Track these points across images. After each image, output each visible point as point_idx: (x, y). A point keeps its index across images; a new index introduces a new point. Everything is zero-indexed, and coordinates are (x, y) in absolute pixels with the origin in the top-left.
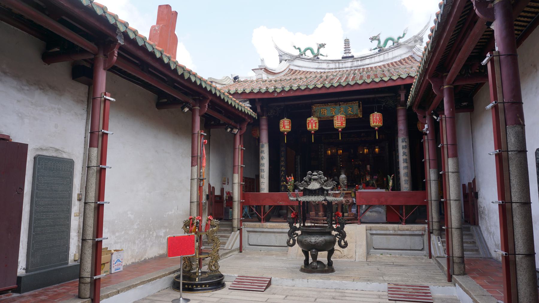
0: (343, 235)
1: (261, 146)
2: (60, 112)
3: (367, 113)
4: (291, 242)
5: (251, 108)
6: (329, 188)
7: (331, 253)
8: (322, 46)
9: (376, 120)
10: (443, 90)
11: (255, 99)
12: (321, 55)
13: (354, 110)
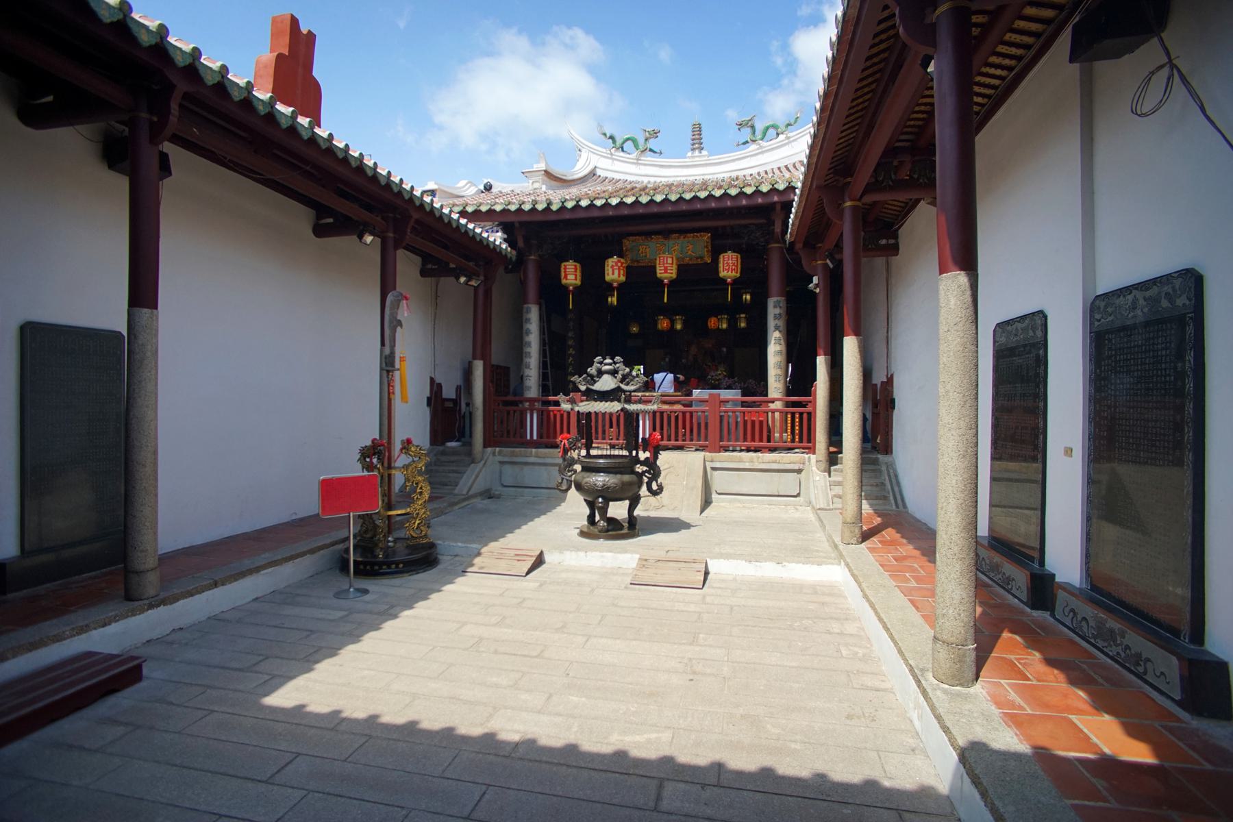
0: (655, 472)
3: (716, 252)
5: (505, 240)
6: (632, 388)
8: (655, 134)
9: (729, 267)
10: (843, 210)
13: (696, 247)
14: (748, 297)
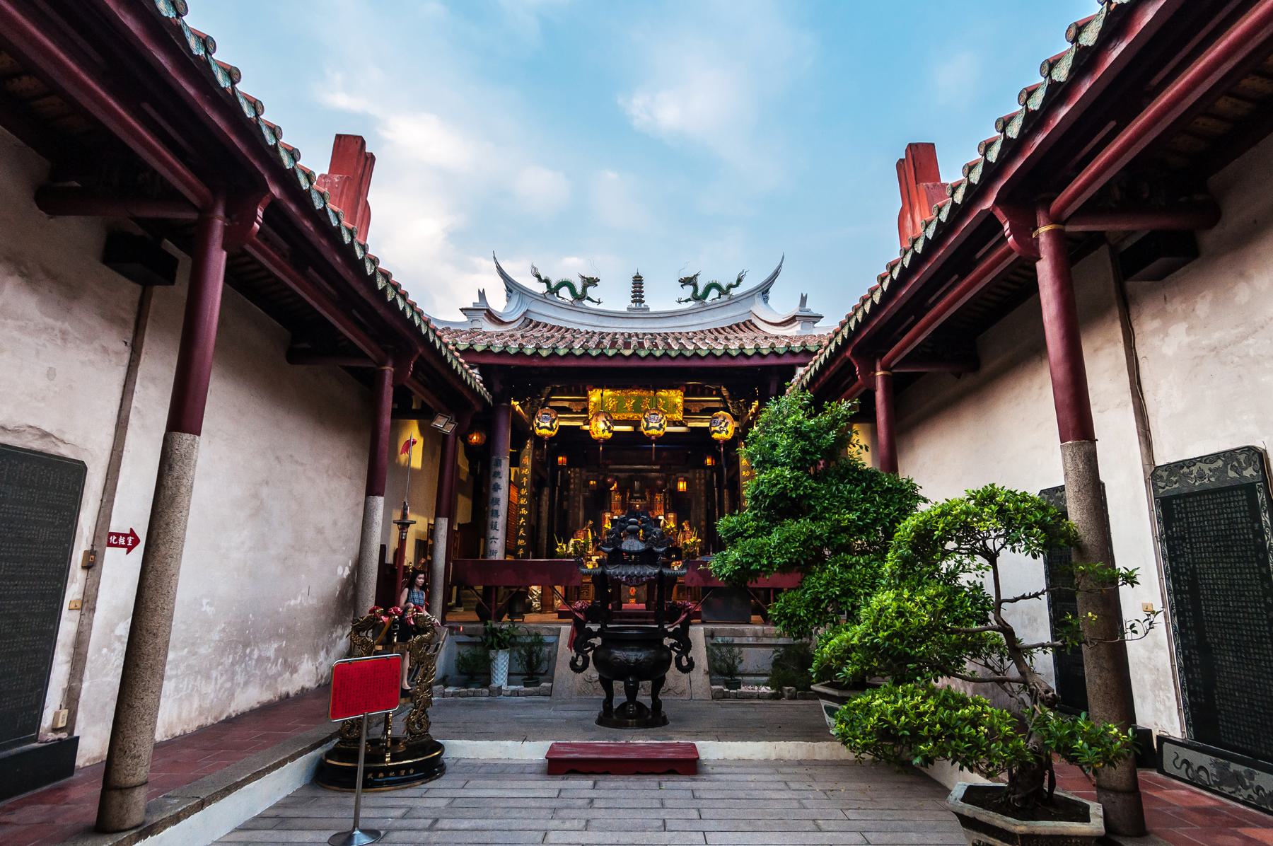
0: (685, 644)
1: (493, 462)
2: (64, 340)
4: (579, 663)
7: (658, 683)
8: (592, 282)
11: (491, 365)
12: (589, 299)
14: (560, 459)
